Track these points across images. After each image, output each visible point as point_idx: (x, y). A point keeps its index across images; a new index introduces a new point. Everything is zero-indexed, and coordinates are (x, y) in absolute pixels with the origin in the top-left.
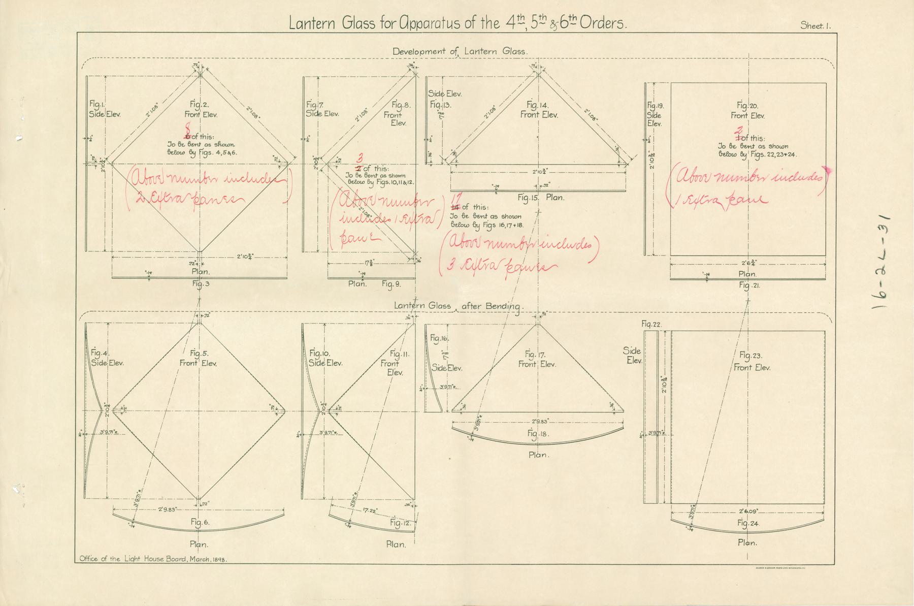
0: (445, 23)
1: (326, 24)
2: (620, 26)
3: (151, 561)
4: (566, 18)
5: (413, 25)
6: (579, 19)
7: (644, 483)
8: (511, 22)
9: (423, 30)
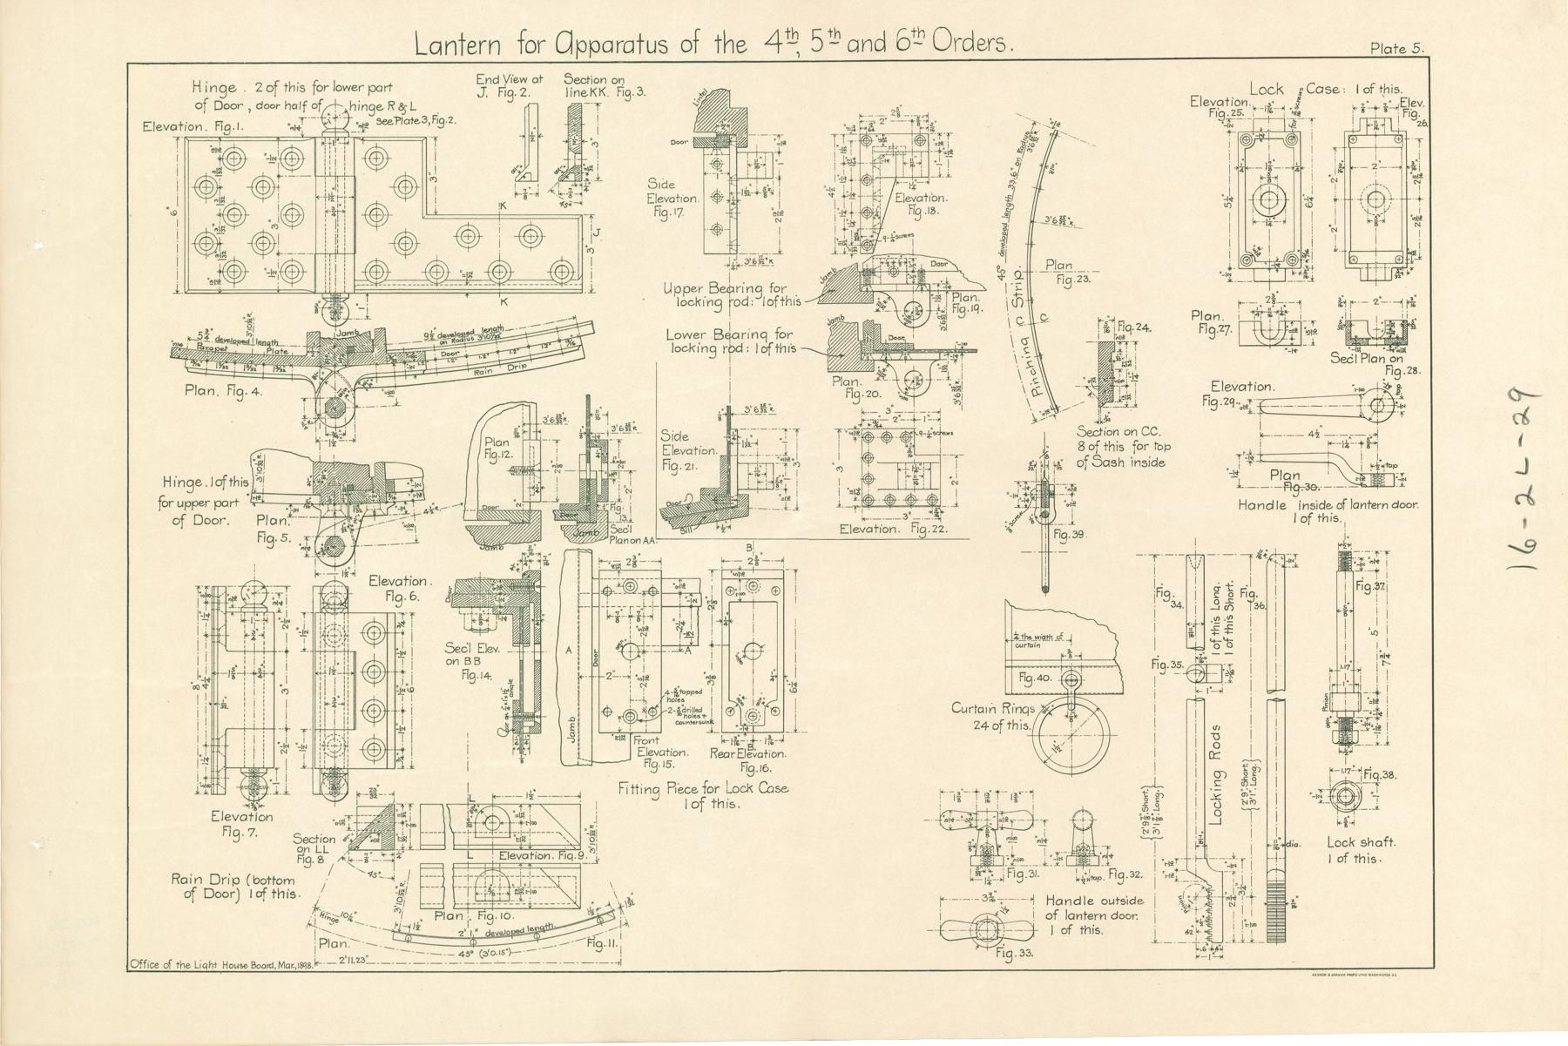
0: (644, 45)
2: (1001, 47)
5: (582, 46)
8: (774, 40)
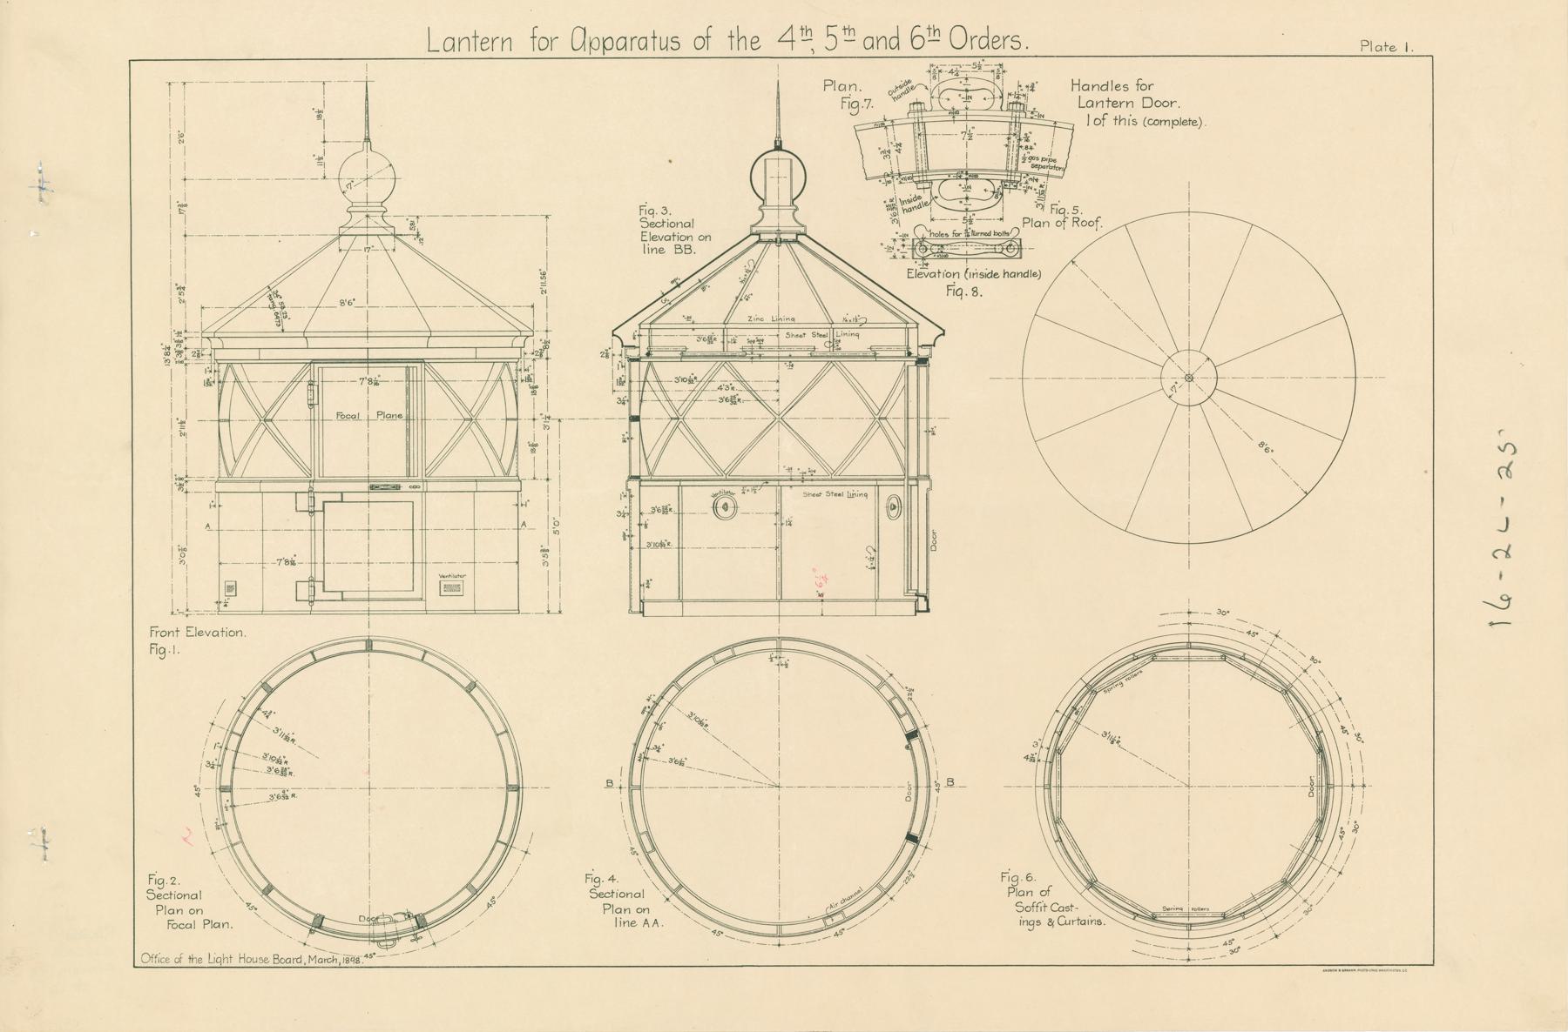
2: (1016, 45)
4: (923, 31)
8: (788, 37)
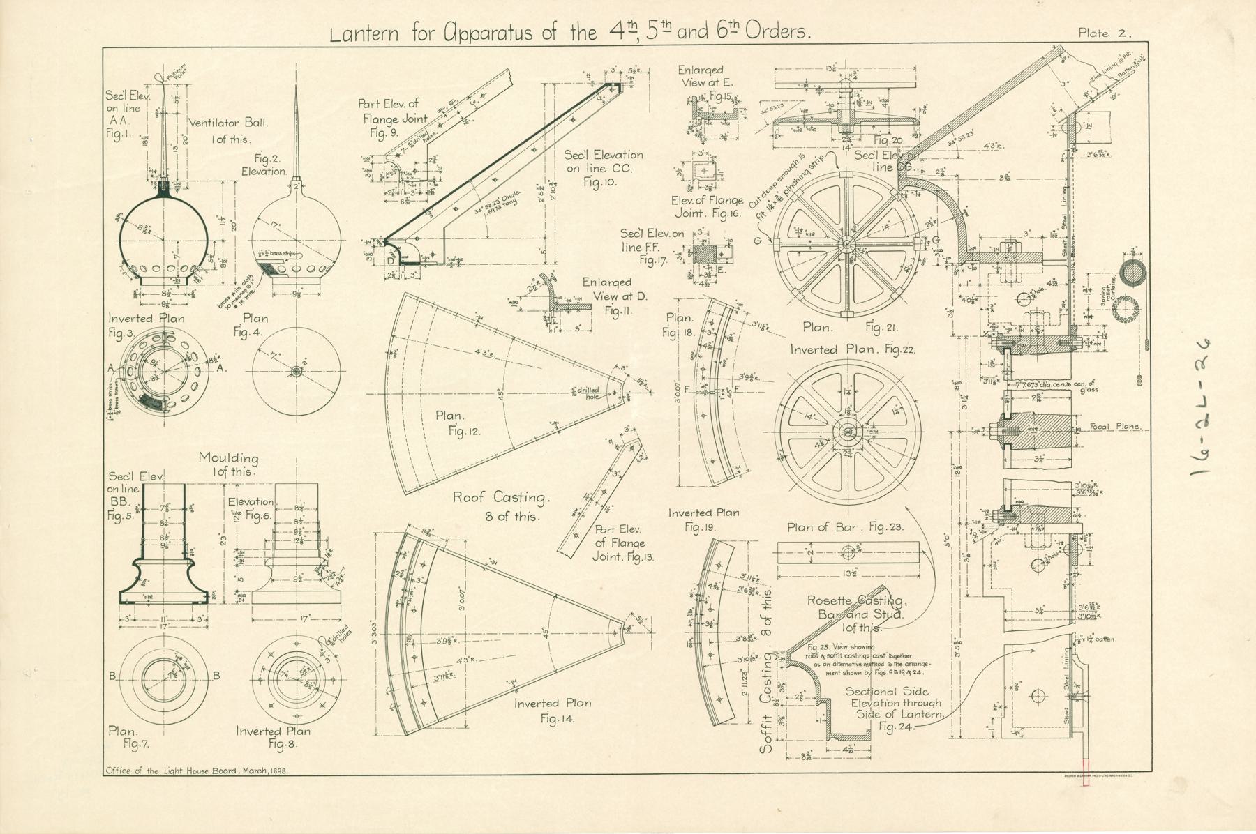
1: (386, 35)
3: (192, 774)
6: (743, 25)
7: (399, 313)
9: (480, 42)
